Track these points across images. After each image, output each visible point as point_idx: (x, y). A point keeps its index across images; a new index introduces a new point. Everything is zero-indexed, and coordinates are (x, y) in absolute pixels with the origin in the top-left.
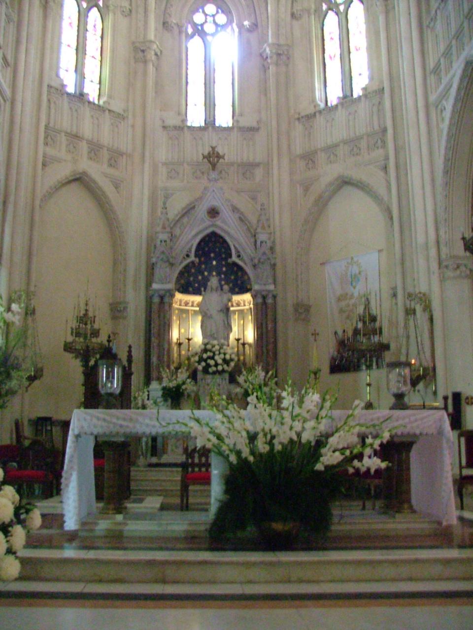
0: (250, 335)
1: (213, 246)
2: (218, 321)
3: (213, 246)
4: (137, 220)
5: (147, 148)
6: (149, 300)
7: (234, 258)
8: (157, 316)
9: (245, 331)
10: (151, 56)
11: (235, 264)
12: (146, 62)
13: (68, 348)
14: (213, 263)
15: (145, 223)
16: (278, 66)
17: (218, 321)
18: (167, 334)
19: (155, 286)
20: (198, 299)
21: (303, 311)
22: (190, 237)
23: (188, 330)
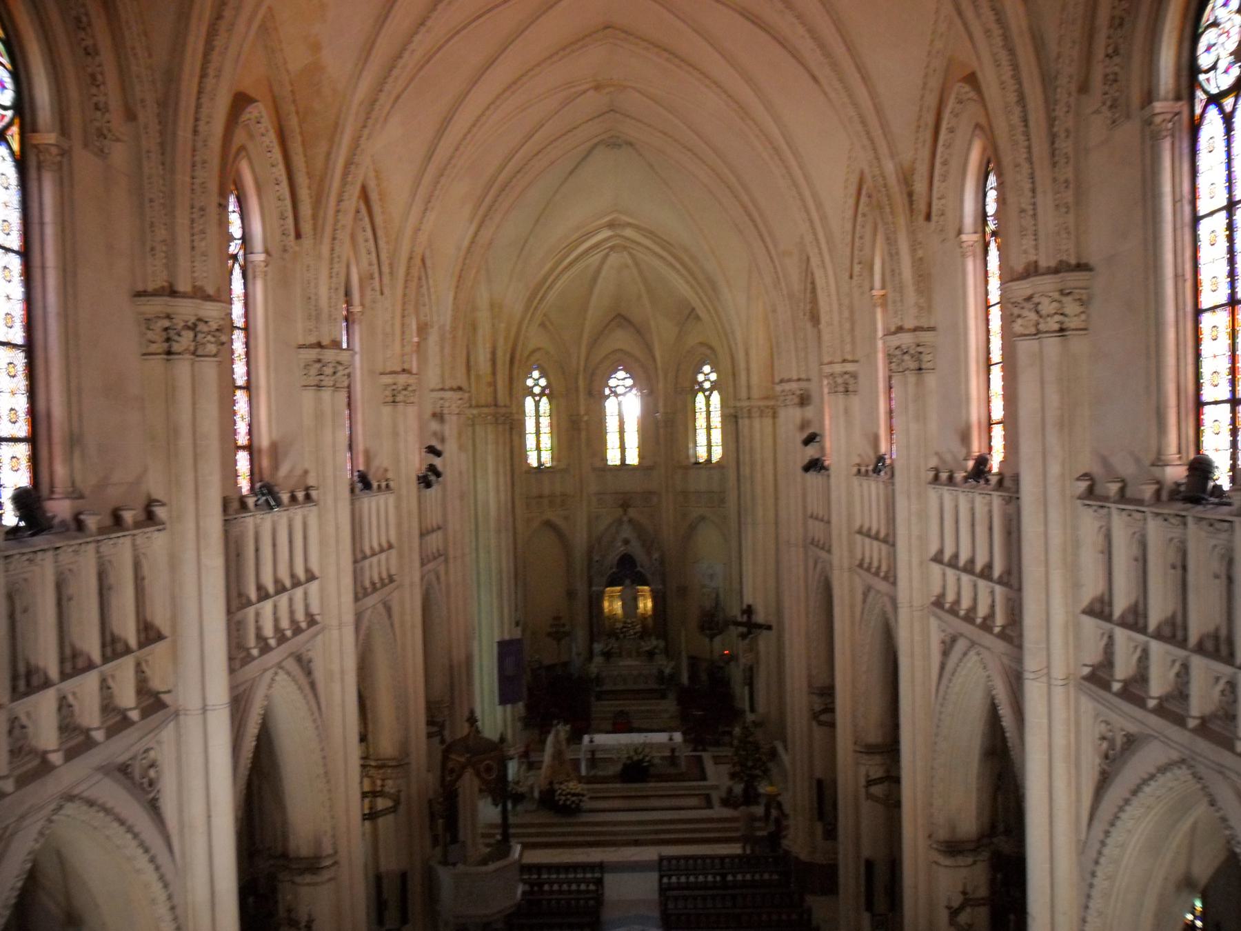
0: (650, 604)
1: (627, 561)
2: (630, 603)
3: (627, 561)
4: (580, 539)
5: (487, 16)
6: (590, 597)
7: (639, 569)
8: (595, 603)
9: (646, 604)
10: (583, 425)
11: (639, 572)
12: (580, 427)
13: (549, 635)
14: (627, 572)
15: (585, 536)
16: (667, 426)
17: (630, 603)
18: (555, 423)
19: (594, 588)
20: (619, 588)
21: (683, 591)
22: (613, 557)
23: (613, 605)
